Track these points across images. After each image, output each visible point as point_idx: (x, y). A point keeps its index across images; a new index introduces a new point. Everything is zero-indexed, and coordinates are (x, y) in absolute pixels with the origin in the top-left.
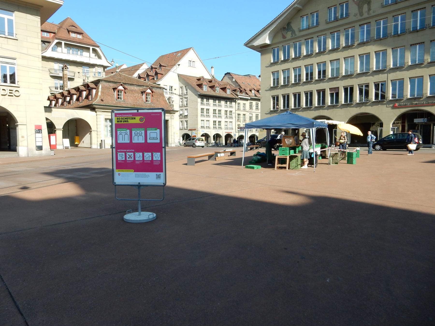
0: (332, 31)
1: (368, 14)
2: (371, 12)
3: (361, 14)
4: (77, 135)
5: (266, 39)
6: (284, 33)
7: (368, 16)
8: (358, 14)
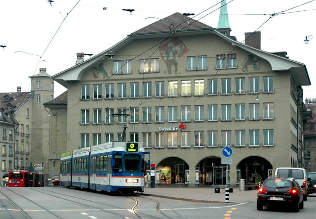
0: (145, 81)
1: (175, 74)
2: (178, 72)
3: (170, 72)
4: (60, 159)
5: (74, 76)
6: (96, 72)
7: (242, 72)
8: (167, 72)
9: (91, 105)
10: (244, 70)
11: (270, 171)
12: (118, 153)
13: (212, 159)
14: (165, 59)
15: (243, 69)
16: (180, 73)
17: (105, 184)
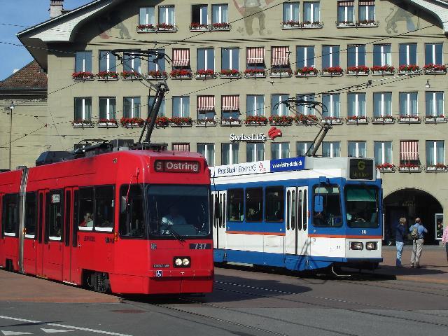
3: (250, 31)
9: (95, 89)
10: (390, 30)
11: (375, 244)
12: (327, 183)
13: (250, 219)
14: (240, 6)
15: (388, 28)
16: (269, 33)
17: (279, 251)
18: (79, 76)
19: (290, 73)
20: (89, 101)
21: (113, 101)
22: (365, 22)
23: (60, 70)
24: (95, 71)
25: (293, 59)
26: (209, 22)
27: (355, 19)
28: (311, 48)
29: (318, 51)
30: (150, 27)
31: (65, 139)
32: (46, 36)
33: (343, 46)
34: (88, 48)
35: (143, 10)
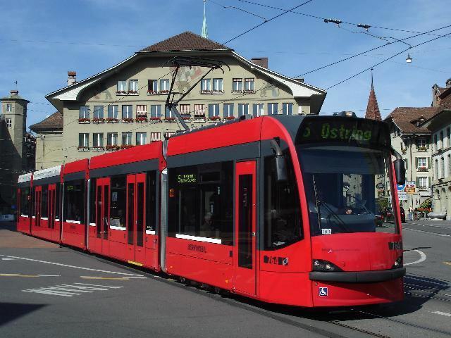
9: (91, 128)
18: (81, 120)
19: (205, 119)
20: (116, 135)
21: (102, 135)
22: (132, 92)
23: (70, 116)
24: (91, 117)
25: (206, 111)
26: (158, 90)
27: (243, 89)
28: (217, 105)
29: (221, 106)
30: (124, 92)
31: (76, 156)
32: (62, 97)
33: (105, 105)
34: (87, 104)
35: (119, 82)
